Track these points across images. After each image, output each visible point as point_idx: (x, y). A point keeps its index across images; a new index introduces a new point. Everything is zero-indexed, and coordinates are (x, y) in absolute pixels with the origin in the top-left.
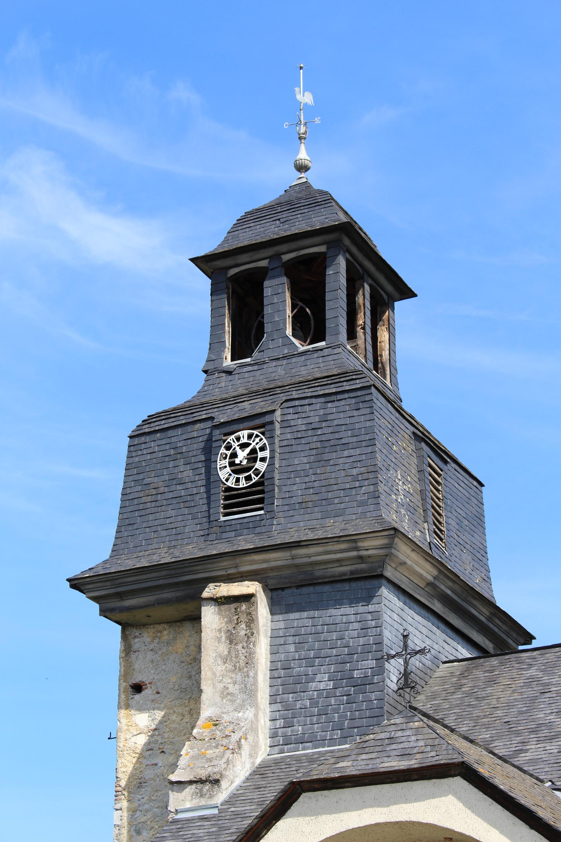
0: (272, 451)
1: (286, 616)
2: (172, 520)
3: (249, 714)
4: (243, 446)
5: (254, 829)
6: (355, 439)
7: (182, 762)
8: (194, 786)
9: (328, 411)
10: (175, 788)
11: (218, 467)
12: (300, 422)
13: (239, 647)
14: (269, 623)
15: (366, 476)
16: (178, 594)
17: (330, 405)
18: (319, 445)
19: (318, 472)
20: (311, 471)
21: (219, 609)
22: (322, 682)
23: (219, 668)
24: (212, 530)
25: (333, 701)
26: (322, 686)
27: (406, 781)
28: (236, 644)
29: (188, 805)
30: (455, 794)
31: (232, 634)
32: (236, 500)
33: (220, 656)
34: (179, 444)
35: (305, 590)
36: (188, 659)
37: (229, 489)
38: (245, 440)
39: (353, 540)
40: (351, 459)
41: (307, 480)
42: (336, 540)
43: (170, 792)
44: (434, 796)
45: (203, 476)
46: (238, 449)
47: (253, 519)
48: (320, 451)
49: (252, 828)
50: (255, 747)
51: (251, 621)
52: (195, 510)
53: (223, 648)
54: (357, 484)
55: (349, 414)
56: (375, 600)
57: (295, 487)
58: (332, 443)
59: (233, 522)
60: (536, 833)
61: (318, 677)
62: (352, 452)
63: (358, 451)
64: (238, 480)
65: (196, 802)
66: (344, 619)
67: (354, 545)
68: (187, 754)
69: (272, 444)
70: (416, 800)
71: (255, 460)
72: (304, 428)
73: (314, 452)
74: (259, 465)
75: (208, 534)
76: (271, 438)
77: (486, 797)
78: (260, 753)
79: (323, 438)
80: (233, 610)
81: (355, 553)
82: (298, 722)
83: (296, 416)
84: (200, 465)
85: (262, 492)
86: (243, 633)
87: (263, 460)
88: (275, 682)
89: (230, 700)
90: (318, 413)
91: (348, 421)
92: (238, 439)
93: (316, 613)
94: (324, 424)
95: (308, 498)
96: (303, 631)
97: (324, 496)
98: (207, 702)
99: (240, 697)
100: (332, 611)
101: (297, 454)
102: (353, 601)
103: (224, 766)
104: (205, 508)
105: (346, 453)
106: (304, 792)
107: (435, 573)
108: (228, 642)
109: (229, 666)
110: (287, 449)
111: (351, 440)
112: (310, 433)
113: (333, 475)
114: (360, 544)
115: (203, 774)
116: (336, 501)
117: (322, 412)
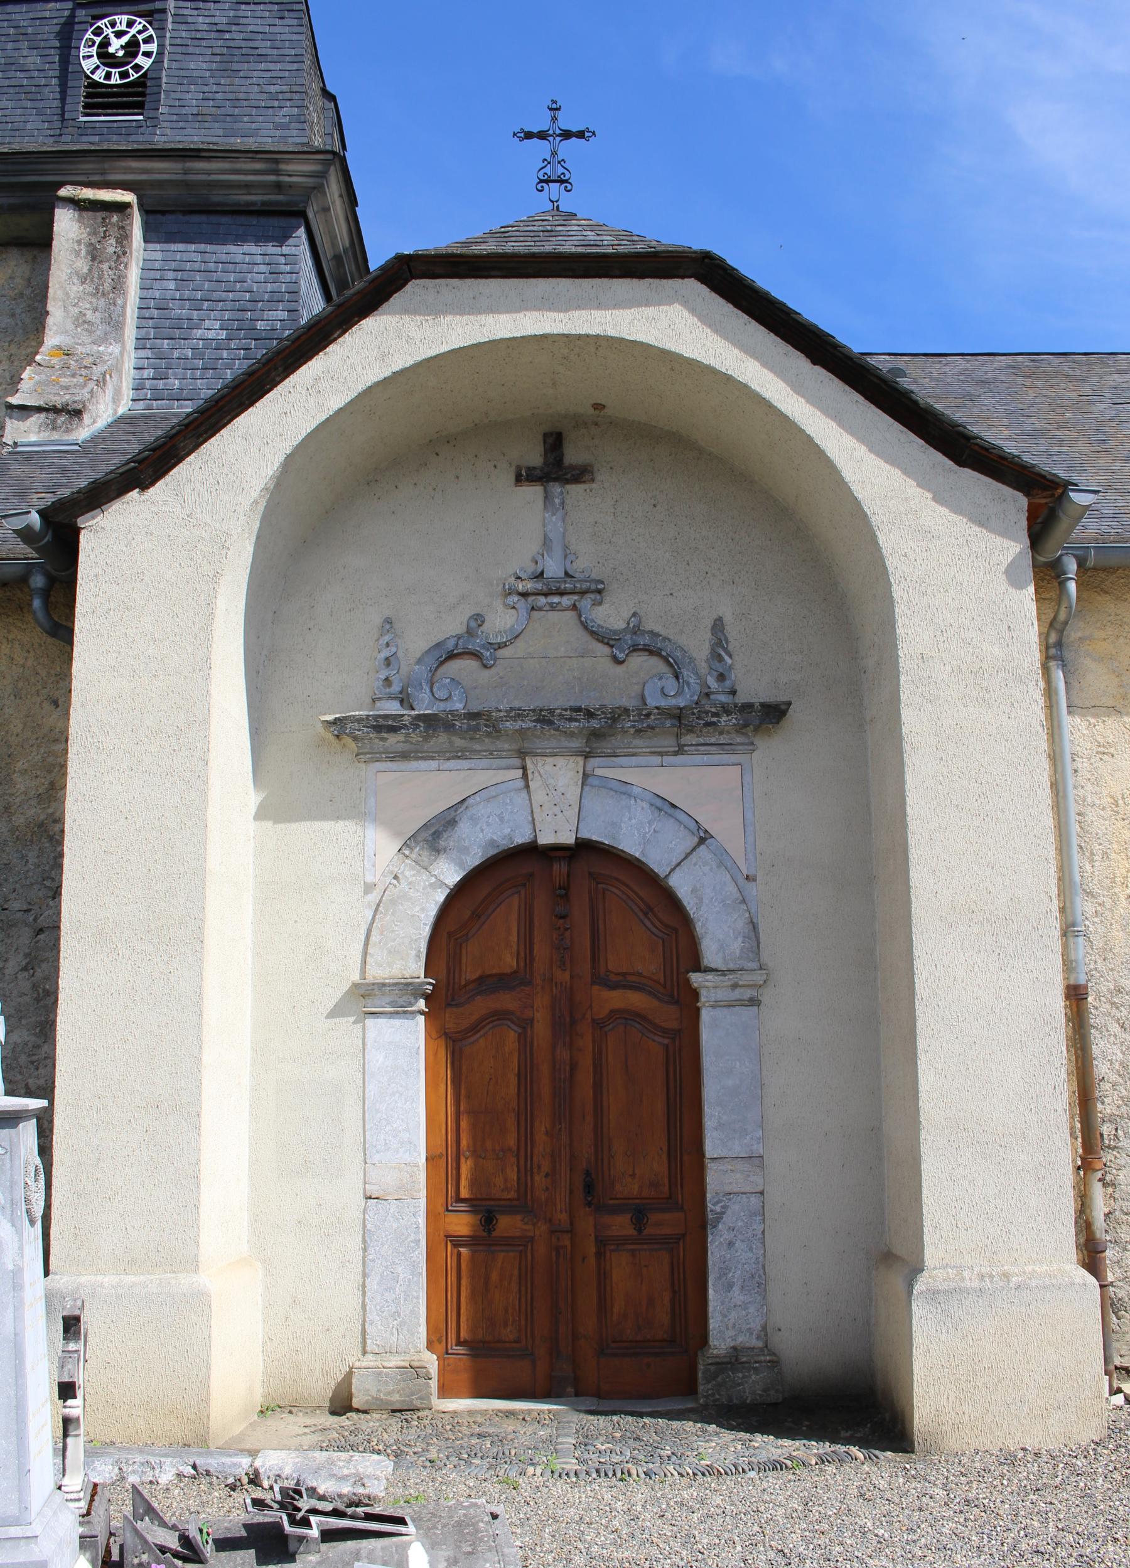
0: (161, 46)
1: (165, 246)
2: (7, 112)
3: (115, 349)
4: (119, 34)
5: (323, 323)
6: (275, 52)
7: (23, 386)
8: (43, 415)
9: (241, 14)
10: (14, 414)
11: (81, 55)
12: (201, 19)
13: (105, 266)
14: (142, 252)
15: (288, 96)
16: (12, 201)
17: (243, 7)
18: (225, 51)
19: (222, 82)
20: (212, 80)
21: (80, 216)
22: (212, 330)
23: (75, 288)
24: (66, 131)
25: (225, 354)
26: (211, 335)
27: (600, 277)
28: (101, 262)
29: (33, 438)
30: (685, 304)
31: (95, 248)
32: (100, 98)
33: (77, 274)
34: (22, 23)
35: (195, 218)
36: (12, 294)
37: (95, 84)
38: (124, 27)
39: (273, 158)
40: (269, 74)
41: (206, 89)
42: (250, 155)
43: (7, 419)
44: (648, 304)
45: (56, 66)
46: (112, 36)
47: (127, 124)
48: (225, 58)
49: (319, 322)
50: (118, 393)
51: (124, 237)
52: (41, 105)
53: (82, 265)
54: (276, 104)
55: (271, 21)
56: (291, 241)
57: (189, 96)
58: (244, 51)
59: (98, 125)
60: (824, 371)
61: (207, 324)
62: (271, 66)
63: (279, 66)
64: (108, 76)
65: (45, 435)
66: (247, 259)
67: (274, 166)
68: (30, 379)
69: (161, 37)
70: (617, 306)
71: (135, 55)
72: (205, 27)
73: (218, 58)
74: (140, 60)
75: (61, 135)
76: (161, 30)
77: (740, 312)
78: (123, 403)
79: (231, 44)
80: (100, 220)
81: (273, 178)
82: (175, 374)
83: (195, 12)
84: (52, 52)
85: (143, 95)
86: (111, 250)
87: (147, 54)
88: (144, 323)
89: (87, 330)
90: (225, 13)
91: (267, 29)
92: (113, 25)
93: (209, 248)
94: (234, 28)
95: (205, 111)
96: (188, 266)
97: (230, 111)
98: (55, 328)
99: (101, 330)
100: (231, 248)
101: (195, 58)
102: (259, 239)
103: (88, 396)
104: (57, 103)
105: (263, 66)
106: (416, 278)
107: (347, 244)
108: (89, 258)
109: (89, 288)
110: (180, 49)
111: (270, 52)
112: (213, 35)
113: (243, 89)
114: (283, 167)
115: (58, 401)
116: (246, 119)
117: (232, 13)
